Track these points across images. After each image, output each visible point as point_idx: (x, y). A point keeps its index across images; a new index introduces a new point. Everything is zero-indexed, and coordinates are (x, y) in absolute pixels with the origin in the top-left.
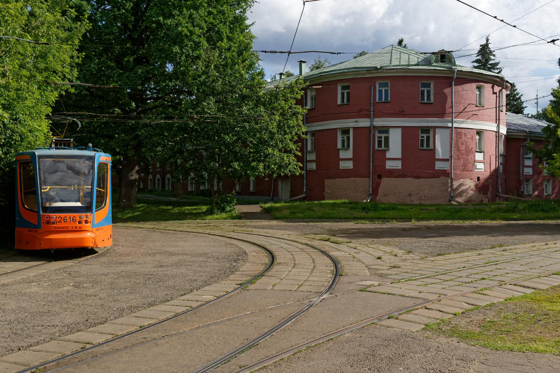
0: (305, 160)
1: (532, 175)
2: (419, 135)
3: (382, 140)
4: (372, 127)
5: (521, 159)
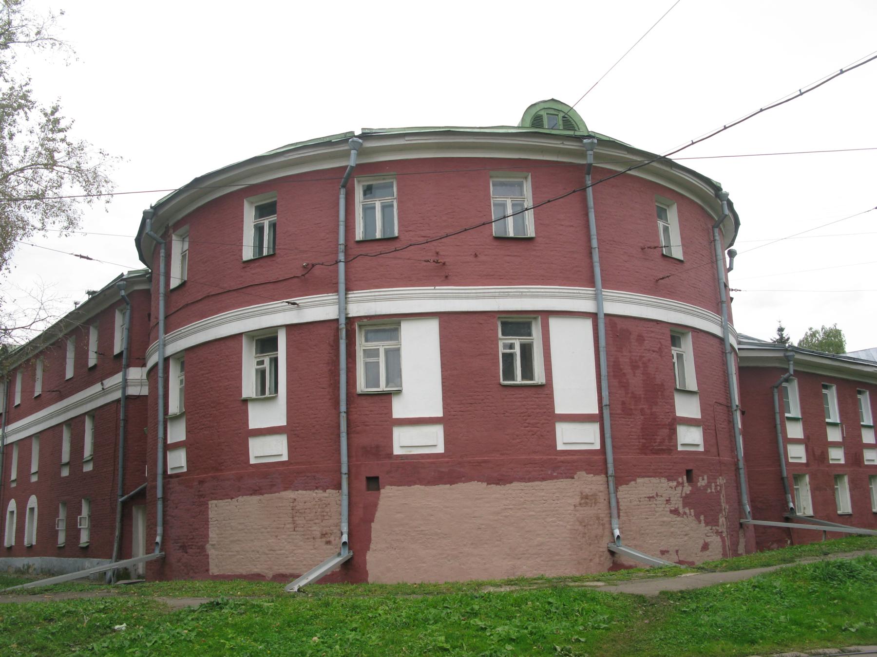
1: (807, 465)
2: (496, 341)
4: (343, 321)
5: (778, 421)
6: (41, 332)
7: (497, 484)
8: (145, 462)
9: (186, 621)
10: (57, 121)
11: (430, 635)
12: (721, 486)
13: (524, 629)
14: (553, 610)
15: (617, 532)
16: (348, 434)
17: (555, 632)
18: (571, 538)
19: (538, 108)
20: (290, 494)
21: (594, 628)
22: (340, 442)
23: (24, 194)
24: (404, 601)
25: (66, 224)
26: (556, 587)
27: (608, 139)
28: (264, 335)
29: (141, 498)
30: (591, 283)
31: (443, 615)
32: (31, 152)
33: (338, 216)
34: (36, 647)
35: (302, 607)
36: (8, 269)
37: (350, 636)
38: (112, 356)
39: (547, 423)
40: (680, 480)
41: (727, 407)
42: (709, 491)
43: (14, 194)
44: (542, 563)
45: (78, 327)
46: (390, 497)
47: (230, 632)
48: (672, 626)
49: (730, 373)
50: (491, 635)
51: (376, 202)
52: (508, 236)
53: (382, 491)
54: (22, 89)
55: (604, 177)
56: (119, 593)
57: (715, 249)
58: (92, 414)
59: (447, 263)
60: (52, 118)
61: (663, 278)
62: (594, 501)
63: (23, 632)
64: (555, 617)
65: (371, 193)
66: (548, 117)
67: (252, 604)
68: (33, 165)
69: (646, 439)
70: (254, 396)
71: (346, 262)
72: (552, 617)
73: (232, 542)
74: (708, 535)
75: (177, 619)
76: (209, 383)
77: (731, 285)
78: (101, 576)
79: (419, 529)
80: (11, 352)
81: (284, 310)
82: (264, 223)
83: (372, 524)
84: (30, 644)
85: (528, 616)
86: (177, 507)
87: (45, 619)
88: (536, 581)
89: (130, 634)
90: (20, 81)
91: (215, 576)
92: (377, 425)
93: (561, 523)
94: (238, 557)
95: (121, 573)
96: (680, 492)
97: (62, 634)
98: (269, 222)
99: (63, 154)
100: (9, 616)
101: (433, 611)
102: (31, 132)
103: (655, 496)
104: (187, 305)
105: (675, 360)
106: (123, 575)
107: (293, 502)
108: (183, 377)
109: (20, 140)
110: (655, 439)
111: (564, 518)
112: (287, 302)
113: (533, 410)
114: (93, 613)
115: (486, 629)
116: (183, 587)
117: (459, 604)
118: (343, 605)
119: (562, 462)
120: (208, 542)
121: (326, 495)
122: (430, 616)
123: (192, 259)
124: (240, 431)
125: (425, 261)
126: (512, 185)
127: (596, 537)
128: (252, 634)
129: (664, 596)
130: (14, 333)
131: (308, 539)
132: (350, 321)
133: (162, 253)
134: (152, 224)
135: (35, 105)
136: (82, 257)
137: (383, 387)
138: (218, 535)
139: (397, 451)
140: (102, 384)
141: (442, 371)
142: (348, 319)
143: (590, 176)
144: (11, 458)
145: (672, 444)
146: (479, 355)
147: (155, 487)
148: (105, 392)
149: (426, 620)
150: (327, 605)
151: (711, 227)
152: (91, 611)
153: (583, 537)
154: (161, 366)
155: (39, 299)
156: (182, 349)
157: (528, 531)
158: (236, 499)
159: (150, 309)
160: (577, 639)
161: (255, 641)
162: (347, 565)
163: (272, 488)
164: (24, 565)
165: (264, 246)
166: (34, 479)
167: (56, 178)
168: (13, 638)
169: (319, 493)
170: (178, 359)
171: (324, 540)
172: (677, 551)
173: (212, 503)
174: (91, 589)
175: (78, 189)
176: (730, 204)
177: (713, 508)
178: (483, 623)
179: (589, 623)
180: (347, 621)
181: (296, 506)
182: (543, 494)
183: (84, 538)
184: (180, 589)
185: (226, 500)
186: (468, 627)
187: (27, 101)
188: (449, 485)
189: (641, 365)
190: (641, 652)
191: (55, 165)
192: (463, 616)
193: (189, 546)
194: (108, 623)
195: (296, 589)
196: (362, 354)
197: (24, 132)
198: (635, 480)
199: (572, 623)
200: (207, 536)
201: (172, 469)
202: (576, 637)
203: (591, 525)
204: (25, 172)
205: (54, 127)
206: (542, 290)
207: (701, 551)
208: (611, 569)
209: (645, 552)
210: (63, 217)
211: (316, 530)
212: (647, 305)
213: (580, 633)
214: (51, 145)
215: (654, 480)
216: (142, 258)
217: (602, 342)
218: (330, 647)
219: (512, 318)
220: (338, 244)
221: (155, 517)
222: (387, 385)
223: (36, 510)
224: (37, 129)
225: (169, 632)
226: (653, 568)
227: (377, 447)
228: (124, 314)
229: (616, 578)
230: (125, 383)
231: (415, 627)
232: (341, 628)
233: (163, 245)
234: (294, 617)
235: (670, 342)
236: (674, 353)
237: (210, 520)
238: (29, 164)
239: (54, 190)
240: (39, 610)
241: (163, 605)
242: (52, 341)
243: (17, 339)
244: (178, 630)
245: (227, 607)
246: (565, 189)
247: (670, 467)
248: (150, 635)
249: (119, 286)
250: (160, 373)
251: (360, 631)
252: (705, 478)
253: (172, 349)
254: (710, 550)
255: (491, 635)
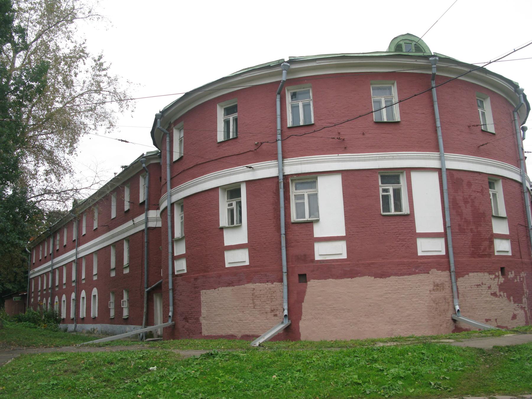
0: (170, 257)
2: (377, 187)
3: (303, 204)
4: (281, 177)
6: (97, 191)
7: (381, 277)
8: (160, 268)
9: (192, 365)
10: (101, 64)
11: (348, 374)
12: (523, 278)
13: (408, 370)
14: (426, 358)
15: (457, 308)
16: (286, 248)
17: (429, 373)
18: (428, 311)
19: (399, 40)
20: (251, 286)
21: (453, 370)
22: (281, 253)
23: (84, 109)
24: (328, 352)
25: (108, 126)
26: (425, 343)
27: (445, 57)
28: (232, 187)
29: (158, 289)
30: (437, 149)
31: (354, 361)
32: (87, 83)
33: (276, 112)
34: (104, 379)
35: (264, 356)
36: (76, 154)
37: (297, 375)
38: (139, 204)
39: (411, 239)
40: (497, 274)
41: (526, 227)
42: (516, 281)
43: (78, 109)
44: (410, 327)
45: (118, 187)
46: (314, 287)
47: (220, 372)
48: (506, 369)
49: (527, 205)
50: (387, 374)
51: (299, 103)
52: (383, 121)
53: (308, 283)
54: (81, 46)
55: (444, 81)
56: (149, 347)
57: (515, 126)
58: (127, 239)
59: (345, 139)
60: (98, 62)
61: (483, 145)
62: (442, 288)
63: (96, 370)
64: (427, 363)
65: (295, 97)
66: (405, 46)
67: (233, 354)
68: (88, 91)
69: (474, 248)
70: (227, 226)
71: (282, 140)
72: (425, 363)
73: (215, 315)
74: (516, 309)
75: (187, 363)
76: (199, 218)
77: (525, 149)
78: (137, 336)
79: (332, 306)
80: (80, 203)
81: (244, 172)
82: (230, 118)
83: (303, 303)
84: (100, 377)
85: (410, 362)
86: (181, 295)
87: (108, 363)
88: (409, 339)
89: (159, 373)
90: (80, 41)
91: (206, 336)
92: (304, 242)
93: (421, 302)
94: (220, 324)
95: (148, 334)
96: (497, 282)
97: (119, 372)
98: (233, 117)
99: (106, 83)
100: (88, 360)
101: (348, 359)
102: (87, 72)
103: (481, 284)
104: (184, 171)
105: (491, 197)
106: (149, 335)
107: (253, 291)
108: (183, 215)
109: (81, 77)
110: (480, 248)
111: (423, 298)
112: (246, 167)
113: (402, 231)
114: (136, 360)
115: (383, 370)
116: (188, 343)
117: (364, 354)
118: (290, 355)
119: (421, 263)
120: (201, 315)
121: (273, 286)
122: (346, 362)
123: (186, 143)
124: (219, 247)
125: (332, 138)
126: (384, 89)
127: (444, 310)
128: (234, 373)
129: (496, 350)
130: (81, 191)
131: (263, 313)
132: (286, 177)
133: (168, 139)
134: (161, 123)
135: (89, 56)
136: (122, 141)
137: (307, 218)
138: (207, 311)
139: (317, 258)
140: (133, 221)
141: (344, 207)
142: (284, 176)
143: (434, 81)
144: (82, 266)
145: (491, 251)
146: (368, 197)
147: (168, 282)
148: (135, 225)
149: (344, 365)
150: (280, 355)
151: (512, 112)
152: (135, 359)
153: (436, 310)
154: (169, 209)
155: (95, 171)
156: (182, 197)
157: (401, 307)
158: (218, 289)
159: (161, 174)
160: (444, 377)
161: (237, 378)
162: (287, 329)
163: (239, 282)
164: (91, 329)
165: (231, 131)
166: (95, 278)
167: (102, 98)
168: (91, 374)
169: (269, 285)
170: (179, 204)
171: (273, 313)
172: (496, 320)
173: (203, 292)
174: (132, 344)
175: (115, 106)
176: (525, 96)
177: (519, 292)
178: (381, 366)
179: (450, 367)
180: (293, 365)
181: (255, 293)
182: (410, 283)
183: (125, 313)
184: (186, 345)
185: (211, 290)
186: (371, 369)
187: (84, 53)
188: (350, 279)
189: (470, 201)
190: (488, 387)
191: (101, 91)
192: (367, 362)
193: (189, 318)
194: (145, 366)
195: (257, 344)
196: (293, 196)
197: (83, 72)
198: (468, 274)
199: (439, 367)
200: (200, 312)
201: (178, 271)
202: (443, 376)
203: (440, 303)
204: (84, 95)
205: (100, 68)
206: (406, 155)
207: (512, 319)
208: (453, 332)
209: (475, 320)
210: (106, 122)
211: (268, 308)
212: (473, 162)
213: (445, 373)
214: (98, 79)
215: (480, 274)
216: (155, 144)
217: (445, 187)
218: (284, 382)
219: (388, 173)
220: (276, 130)
221: (168, 301)
222: (310, 217)
223: (97, 296)
224: (90, 70)
225: (183, 372)
226: (480, 331)
227: (305, 255)
228: (145, 178)
229: (460, 337)
230: (147, 220)
231: (337, 369)
232: (290, 370)
233: (168, 135)
234: (260, 362)
235: (488, 186)
236: (491, 193)
237: (202, 302)
238: (86, 91)
239: (101, 105)
240: (104, 357)
241: (178, 355)
242: (103, 196)
243: (83, 195)
244: (188, 371)
245: (218, 356)
246: (418, 90)
247: (490, 266)
248: (172, 373)
249: (141, 161)
250: (169, 213)
251: (303, 372)
252: (513, 272)
253: (176, 198)
254: (517, 319)
255: (387, 374)
